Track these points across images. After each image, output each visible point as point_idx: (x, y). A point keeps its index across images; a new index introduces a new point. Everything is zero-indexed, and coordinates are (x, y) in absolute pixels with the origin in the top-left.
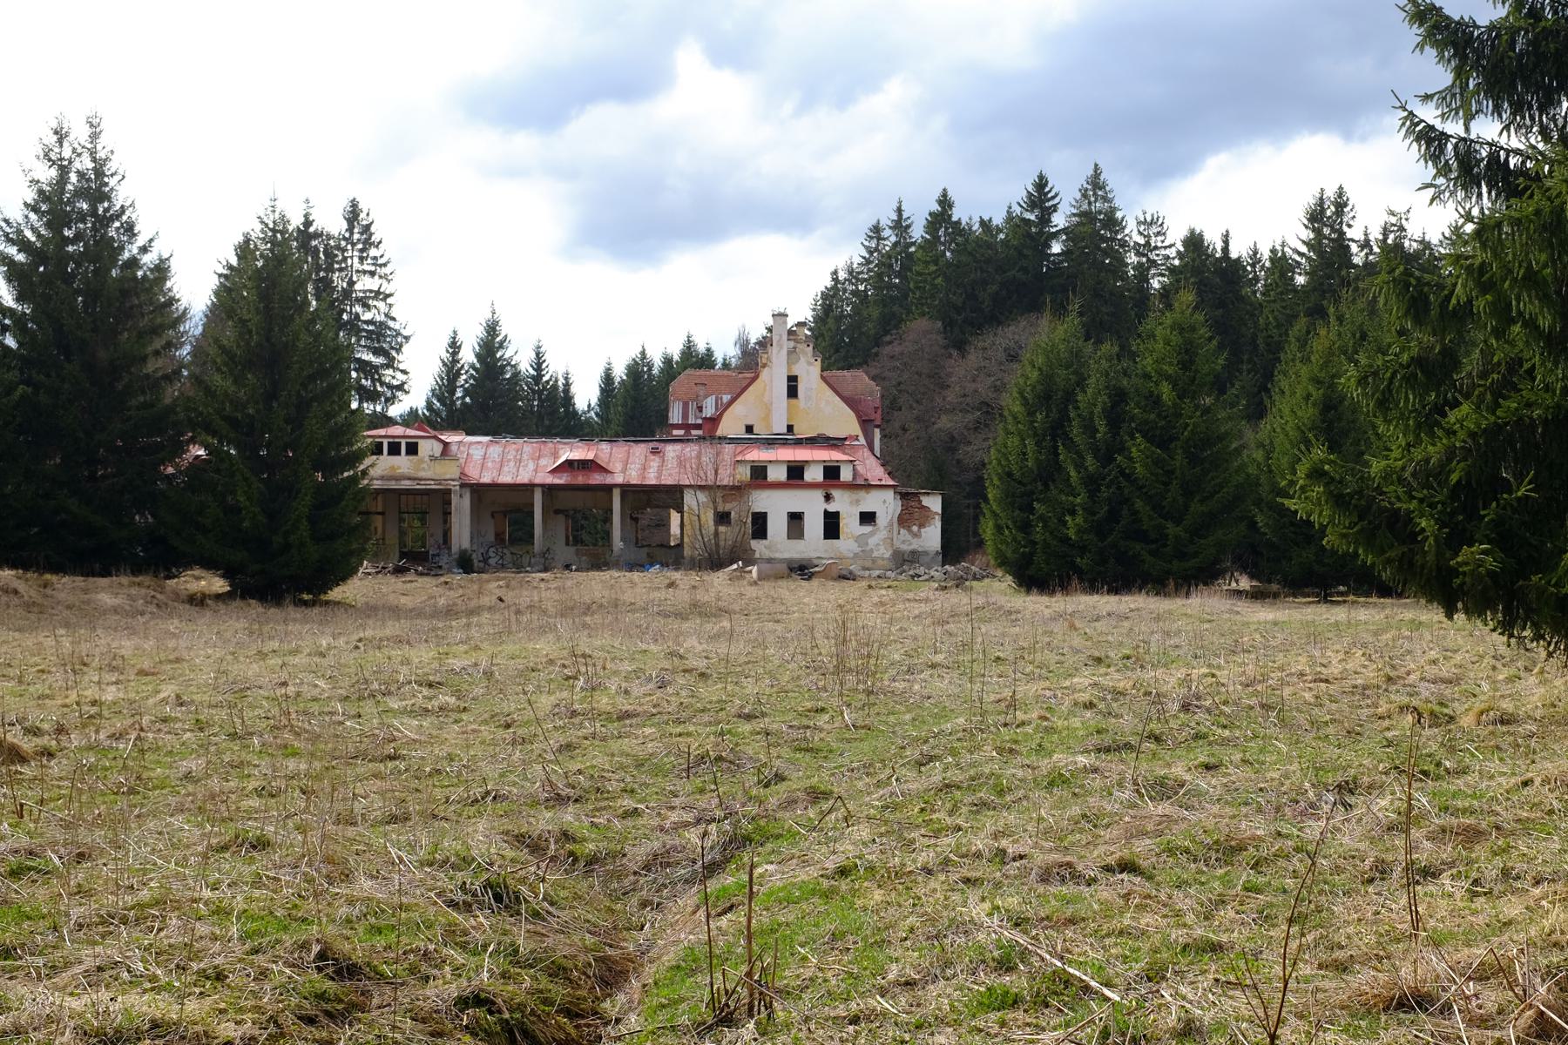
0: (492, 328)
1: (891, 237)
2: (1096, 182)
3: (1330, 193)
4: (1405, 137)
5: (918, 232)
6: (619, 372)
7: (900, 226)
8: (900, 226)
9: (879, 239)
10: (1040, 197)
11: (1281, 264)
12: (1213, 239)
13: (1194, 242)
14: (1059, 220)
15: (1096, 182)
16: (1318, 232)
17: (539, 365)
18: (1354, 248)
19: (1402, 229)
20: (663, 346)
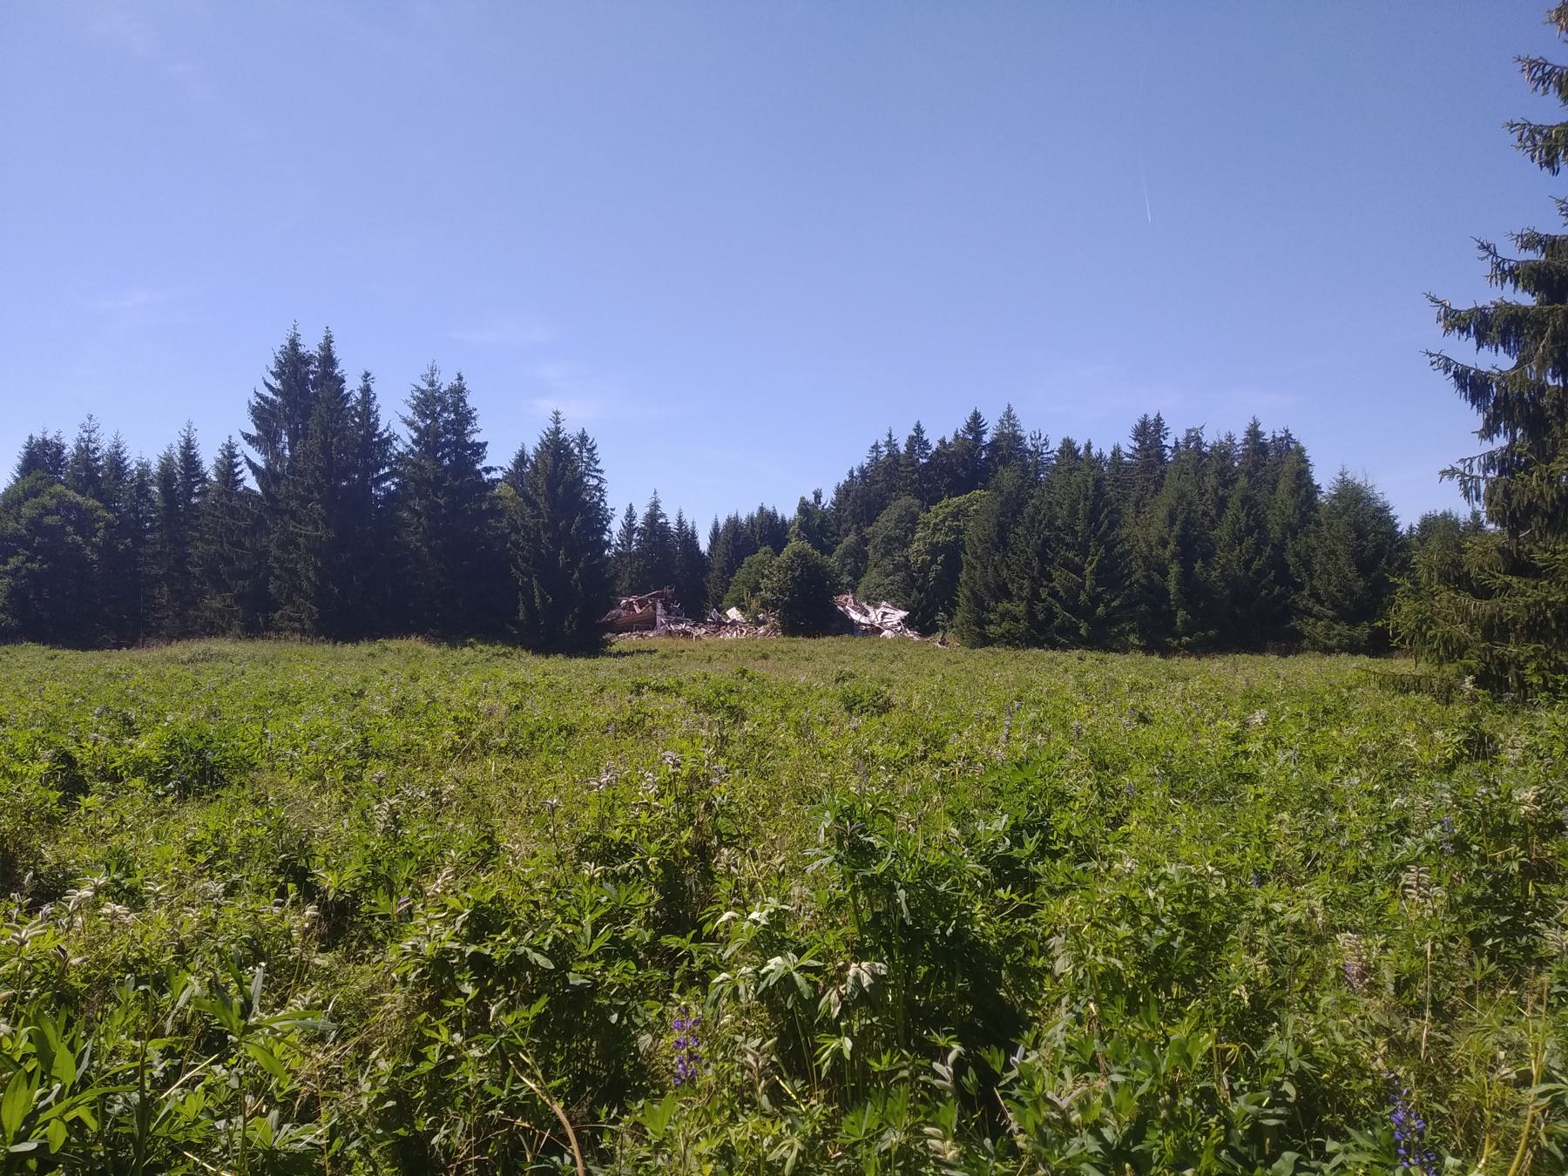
0: (655, 506)
1: (885, 451)
2: (1009, 415)
3: (1152, 417)
4: (242, 480)
5: (903, 449)
6: (722, 522)
7: (890, 443)
8: (890, 443)
9: (878, 452)
10: (976, 424)
11: (144, 470)
12: (1080, 444)
13: (1068, 445)
14: (987, 438)
15: (1009, 415)
16: (1142, 443)
17: (680, 523)
18: (1168, 452)
19: (1199, 438)
20: (746, 510)
